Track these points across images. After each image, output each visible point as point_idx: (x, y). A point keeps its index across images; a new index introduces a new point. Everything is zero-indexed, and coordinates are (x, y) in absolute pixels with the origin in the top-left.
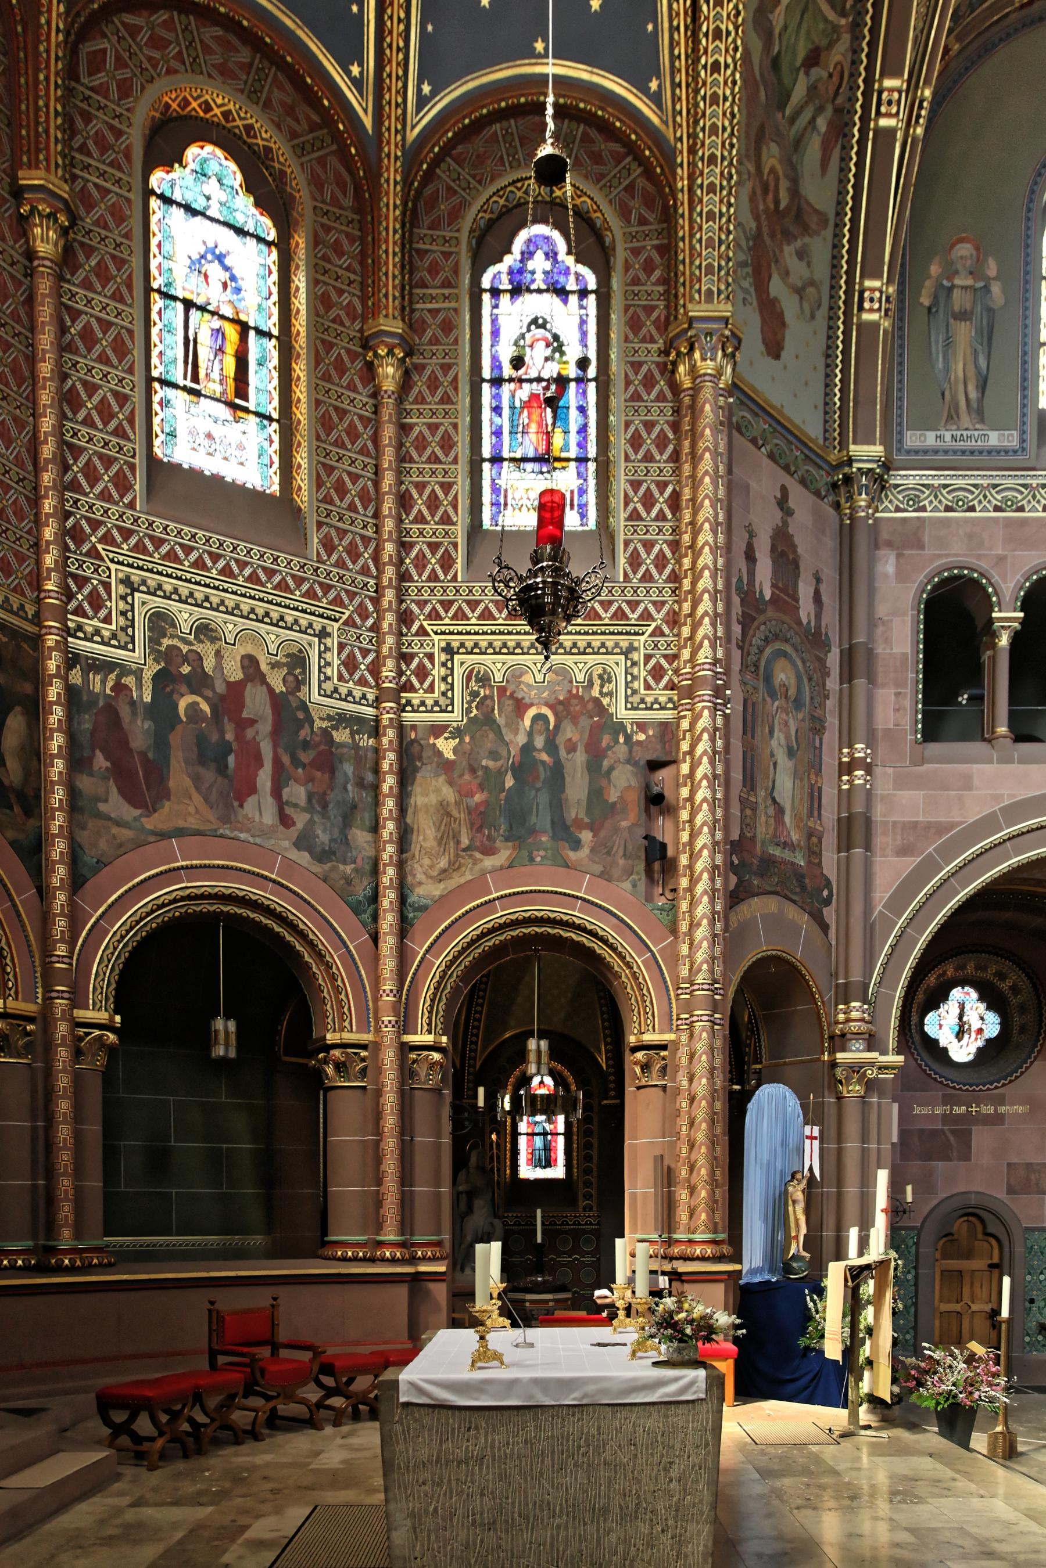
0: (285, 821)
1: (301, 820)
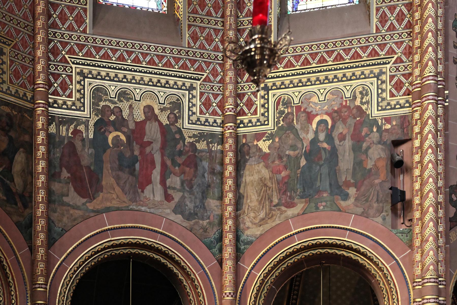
0: (168, 198)
1: (177, 196)
